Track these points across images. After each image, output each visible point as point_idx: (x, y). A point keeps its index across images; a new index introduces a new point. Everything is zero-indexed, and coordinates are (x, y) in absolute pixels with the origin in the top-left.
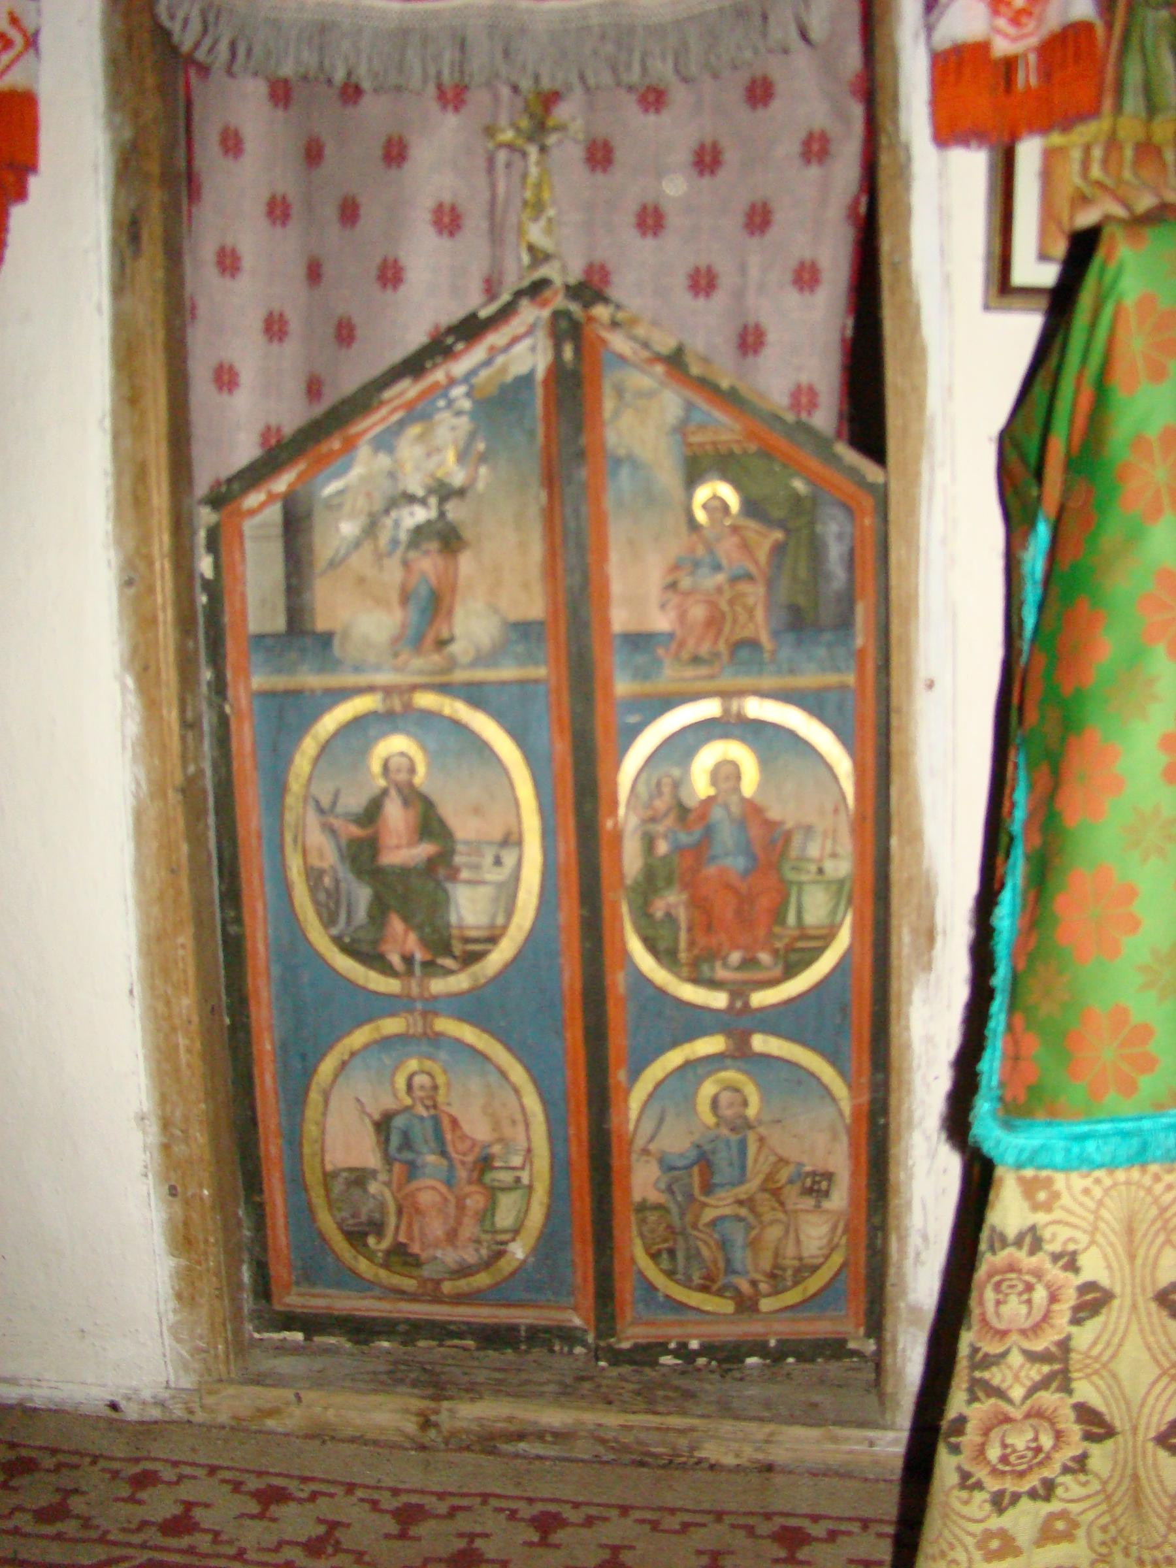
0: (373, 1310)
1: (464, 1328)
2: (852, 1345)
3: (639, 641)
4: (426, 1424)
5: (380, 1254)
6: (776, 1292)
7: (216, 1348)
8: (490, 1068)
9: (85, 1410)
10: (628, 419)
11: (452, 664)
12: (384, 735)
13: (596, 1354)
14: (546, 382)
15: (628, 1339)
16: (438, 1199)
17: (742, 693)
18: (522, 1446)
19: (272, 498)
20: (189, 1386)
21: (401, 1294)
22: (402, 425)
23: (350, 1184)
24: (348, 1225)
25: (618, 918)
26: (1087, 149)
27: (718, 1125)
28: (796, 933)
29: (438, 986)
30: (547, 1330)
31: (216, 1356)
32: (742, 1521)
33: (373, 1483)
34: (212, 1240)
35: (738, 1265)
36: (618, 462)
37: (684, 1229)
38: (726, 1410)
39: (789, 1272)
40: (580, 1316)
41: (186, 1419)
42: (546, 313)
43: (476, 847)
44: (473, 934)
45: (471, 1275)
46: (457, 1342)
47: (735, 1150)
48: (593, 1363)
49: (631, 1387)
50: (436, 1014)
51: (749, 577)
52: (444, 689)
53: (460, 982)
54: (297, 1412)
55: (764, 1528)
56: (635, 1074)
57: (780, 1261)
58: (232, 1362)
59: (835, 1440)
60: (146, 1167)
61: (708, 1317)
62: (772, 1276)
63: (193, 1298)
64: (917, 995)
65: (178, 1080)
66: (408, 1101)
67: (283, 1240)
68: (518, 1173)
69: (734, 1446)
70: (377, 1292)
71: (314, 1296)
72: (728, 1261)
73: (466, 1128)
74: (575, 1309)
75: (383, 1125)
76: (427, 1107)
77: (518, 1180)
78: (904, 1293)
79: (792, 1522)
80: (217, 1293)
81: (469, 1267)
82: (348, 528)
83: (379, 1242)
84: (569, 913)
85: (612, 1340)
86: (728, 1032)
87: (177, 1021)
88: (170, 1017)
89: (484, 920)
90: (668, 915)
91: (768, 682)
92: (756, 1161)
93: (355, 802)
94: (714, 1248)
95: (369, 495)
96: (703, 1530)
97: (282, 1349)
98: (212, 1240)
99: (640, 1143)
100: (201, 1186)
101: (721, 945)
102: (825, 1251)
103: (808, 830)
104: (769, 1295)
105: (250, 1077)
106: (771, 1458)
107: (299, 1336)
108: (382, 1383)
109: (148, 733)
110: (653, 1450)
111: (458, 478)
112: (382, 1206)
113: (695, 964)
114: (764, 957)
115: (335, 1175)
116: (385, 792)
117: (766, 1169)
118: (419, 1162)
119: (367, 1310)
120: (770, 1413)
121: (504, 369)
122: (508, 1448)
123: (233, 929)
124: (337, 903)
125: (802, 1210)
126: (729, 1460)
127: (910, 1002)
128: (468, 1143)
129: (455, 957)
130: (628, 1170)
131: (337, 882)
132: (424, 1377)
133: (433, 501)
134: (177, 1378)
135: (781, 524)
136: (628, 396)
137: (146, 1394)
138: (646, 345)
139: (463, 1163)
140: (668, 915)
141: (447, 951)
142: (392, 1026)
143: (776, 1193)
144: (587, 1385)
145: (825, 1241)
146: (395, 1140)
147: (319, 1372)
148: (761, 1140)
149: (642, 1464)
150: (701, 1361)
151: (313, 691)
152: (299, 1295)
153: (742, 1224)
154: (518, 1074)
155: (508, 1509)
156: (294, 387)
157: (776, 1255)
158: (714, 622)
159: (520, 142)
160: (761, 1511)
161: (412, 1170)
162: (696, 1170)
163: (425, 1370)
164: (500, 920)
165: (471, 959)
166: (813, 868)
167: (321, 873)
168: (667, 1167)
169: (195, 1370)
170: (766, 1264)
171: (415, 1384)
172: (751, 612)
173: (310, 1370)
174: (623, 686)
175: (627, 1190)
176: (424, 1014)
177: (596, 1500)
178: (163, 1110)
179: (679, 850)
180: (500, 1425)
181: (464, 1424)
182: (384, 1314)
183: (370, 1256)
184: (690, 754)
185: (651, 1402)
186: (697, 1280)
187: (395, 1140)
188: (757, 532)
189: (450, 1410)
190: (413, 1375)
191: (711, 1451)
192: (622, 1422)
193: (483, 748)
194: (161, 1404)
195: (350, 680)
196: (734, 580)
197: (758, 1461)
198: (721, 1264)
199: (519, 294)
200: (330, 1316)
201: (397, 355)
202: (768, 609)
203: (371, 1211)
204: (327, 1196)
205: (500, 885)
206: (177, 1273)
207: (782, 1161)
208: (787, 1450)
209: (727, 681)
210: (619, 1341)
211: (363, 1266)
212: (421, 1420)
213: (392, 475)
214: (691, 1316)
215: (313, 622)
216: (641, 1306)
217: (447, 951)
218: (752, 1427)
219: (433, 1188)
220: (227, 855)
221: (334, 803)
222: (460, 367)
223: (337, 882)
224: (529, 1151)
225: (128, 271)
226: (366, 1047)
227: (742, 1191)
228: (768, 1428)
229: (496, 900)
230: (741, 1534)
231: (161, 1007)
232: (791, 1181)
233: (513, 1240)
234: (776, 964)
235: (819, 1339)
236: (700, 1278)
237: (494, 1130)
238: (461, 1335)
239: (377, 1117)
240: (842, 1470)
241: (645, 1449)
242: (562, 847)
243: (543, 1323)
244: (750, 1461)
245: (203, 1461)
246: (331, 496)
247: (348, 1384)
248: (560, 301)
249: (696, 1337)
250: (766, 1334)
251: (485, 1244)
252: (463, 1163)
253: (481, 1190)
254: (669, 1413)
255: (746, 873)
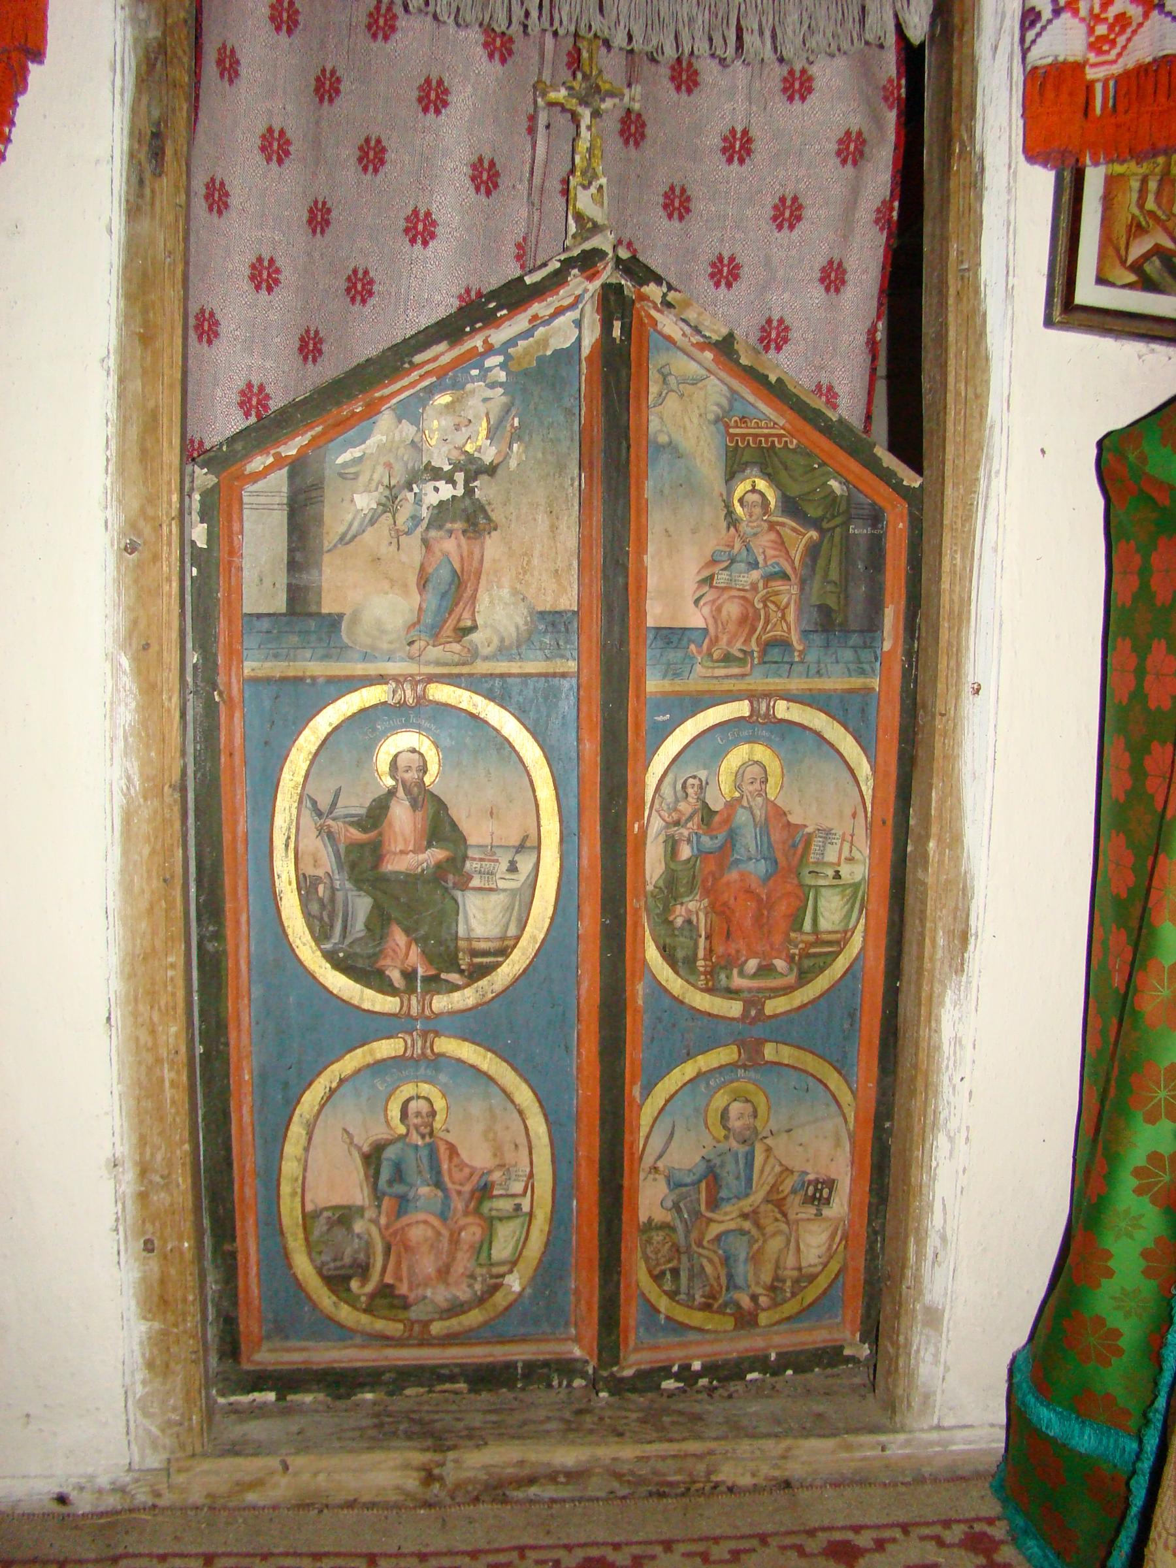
0: (356, 1360)
1: (457, 1370)
2: (847, 1352)
3: (672, 636)
4: (429, 1477)
5: (363, 1299)
6: (775, 1304)
7: (190, 1419)
8: (494, 1090)
9: (25, 1508)
10: (672, 403)
11: (474, 654)
12: (393, 730)
13: (594, 1385)
14: (589, 359)
15: (630, 1366)
16: (430, 1233)
17: (768, 695)
18: (533, 1490)
19: (279, 462)
20: (156, 1465)
21: (385, 1339)
22: (430, 391)
23: (332, 1224)
24: (329, 1269)
25: (637, 924)
26: (1144, 181)
27: (726, 1137)
28: (812, 938)
29: (440, 1003)
30: (546, 1364)
31: (190, 1429)
32: (788, 1541)
33: (394, 1550)
34: (191, 1298)
35: (739, 1280)
36: (661, 448)
37: (689, 1246)
38: (737, 1429)
39: (789, 1283)
40: (581, 1347)
41: (150, 1503)
42: (597, 284)
43: (490, 852)
44: (483, 945)
45: (464, 1312)
46: (447, 1386)
47: (742, 1162)
48: (593, 1396)
49: (635, 1416)
50: (437, 1034)
51: (785, 576)
52: (473, 683)
53: (465, 998)
54: (284, 1481)
55: (813, 1545)
56: (648, 1090)
57: (780, 1272)
58: (205, 1435)
59: (849, 1447)
60: (117, 1220)
61: (708, 1336)
62: (772, 1288)
63: (167, 1366)
64: (949, 997)
65: (161, 1119)
66: (402, 1130)
67: (255, 1291)
68: (517, 1201)
69: (752, 1465)
70: (358, 1340)
71: (288, 1350)
72: (730, 1277)
73: (464, 1155)
74: (578, 1340)
75: (372, 1158)
76: (423, 1136)
77: (518, 1207)
78: (921, 1293)
79: (837, 1536)
80: (194, 1357)
81: (462, 1304)
82: (364, 502)
83: (363, 1285)
84: (590, 922)
85: (615, 1369)
86: (741, 1044)
87: (163, 1052)
88: (154, 1048)
89: (495, 932)
90: (689, 922)
91: (796, 684)
92: (762, 1171)
93: (356, 803)
94: (718, 1265)
95: (389, 466)
96: (754, 1556)
97: (258, 1412)
98: (191, 1298)
99: (648, 1161)
100: (180, 1239)
101: (738, 951)
102: (824, 1259)
103: (828, 833)
104: (768, 1308)
105: (226, 1114)
106: (787, 1473)
107: (271, 1396)
108: (373, 1438)
109: (144, 723)
110: (670, 1479)
111: (489, 455)
112: (369, 1246)
113: (711, 973)
114: (780, 964)
115: (316, 1214)
116: (392, 793)
117: (771, 1180)
118: (411, 1195)
119: (351, 1361)
120: (780, 1428)
121: (545, 342)
122: (519, 1494)
123: (211, 946)
124: (332, 915)
125: (803, 1220)
126: (746, 1481)
127: (941, 1004)
128: (467, 1171)
129: (461, 972)
130: (635, 1190)
131: (333, 890)
132: (416, 1428)
133: (460, 477)
134: (143, 1457)
135: (815, 524)
136: (672, 380)
137: (103, 1481)
138: (697, 330)
139: (459, 1193)
140: (689, 922)
141: (452, 964)
142: (386, 1048)
143: (780, 1204)
144: (588, 1418)
145: (824, 1248)
146: (386, 1173)
147: (299, 1433)
148: (769, 1150)
149: (662, 1495)
150: (703, 1382)
151: (314, 679)
152: (270, 1350)
153: (745, 1238)
154: (524, 1095)
155: (551, 1560)
156: (286, 343)
157: (777, 1267)
158: (748, 621)
159: (572, 104)
160: (802, 1528)
161: (403, 1204)
162: (703, 1185)
163: (412, 1420)
164: (512, 931)
165: (486, 971)
166: (830, 872)
167: (316, 880)
168: (674, 1184)
169: (164, 1447)
170: (766, 1277)
171: (409, 1436)
172: (783, 610)
173: (288, 1434)
174: (654, 684)
175: (635, 1211)
176: (424, 1035)
177: (635, 1539)
178: (142, 1154)
179: (702, 854)
180: (510, 1470)
181: (470, 1474)
182: (371, 1364)
183: (352, 1303)
184: (720, 754)
185: (661, 1428)
186: (699, 1299)
187: (386, 1173)
188: (794, 530)
189: (456, 1461)
190: (402, 1427)
191: (727, 1474)
192: (638, 1453)
193: (504, 745)
194: (122, 1490)
195: (360, 669)
196: (769, 578)
197: (775, 1479)
198: (724, 1281)
199: (568, 264)
200: (307, 1371)
201: (426, 319)
202: (800, 611)
203: (357, 1252)
204: (307, 1239)
205: (513, 893)
206: (150, 1338)
207: (787, 1171)
208: (803, 1463)
209: (758, 681)
210: (622, 1369)
211: (345, 1313)
212: (423, 1474)
213: (416, 446)
214: (692, 1336)
215: (319, 604)
216: (642, 1330)
217: (452, 964)
218: (769, 1444)
219: (425, 1222)
220: (208, 863)
221: (334, 804)
222: (499, 336)
223: (333, 890)
224: (531, 1175)
225: (148, 192)
226: (358, 1072)
227: (746, 1205)
228: (788, 1442)
229: (510, 908)
230: (793, 1554)
231: (144, 1037)
232: (794, 1191)
233: (511, 1271)
234: (791, 969)
235: (819, 1349)
236: (703, 1296)
237: (495, 1155)
238: (452, 1378)
239: (366, 1149)
240: (857, 1478)
241: (662, 1479)
242: (585, 851)
243: (541, 1357)
244: (766, 1478)
245: (194, 1549)
246: (345, 465)
247: (337, 1444)
248: (608, 274)
249: (698, 1357)
250: (767, 1348)
251: (479, 1279)
252: (459, 1193)
253: (478, 1221)
254: (684, 1439)
255: (768, 877)
